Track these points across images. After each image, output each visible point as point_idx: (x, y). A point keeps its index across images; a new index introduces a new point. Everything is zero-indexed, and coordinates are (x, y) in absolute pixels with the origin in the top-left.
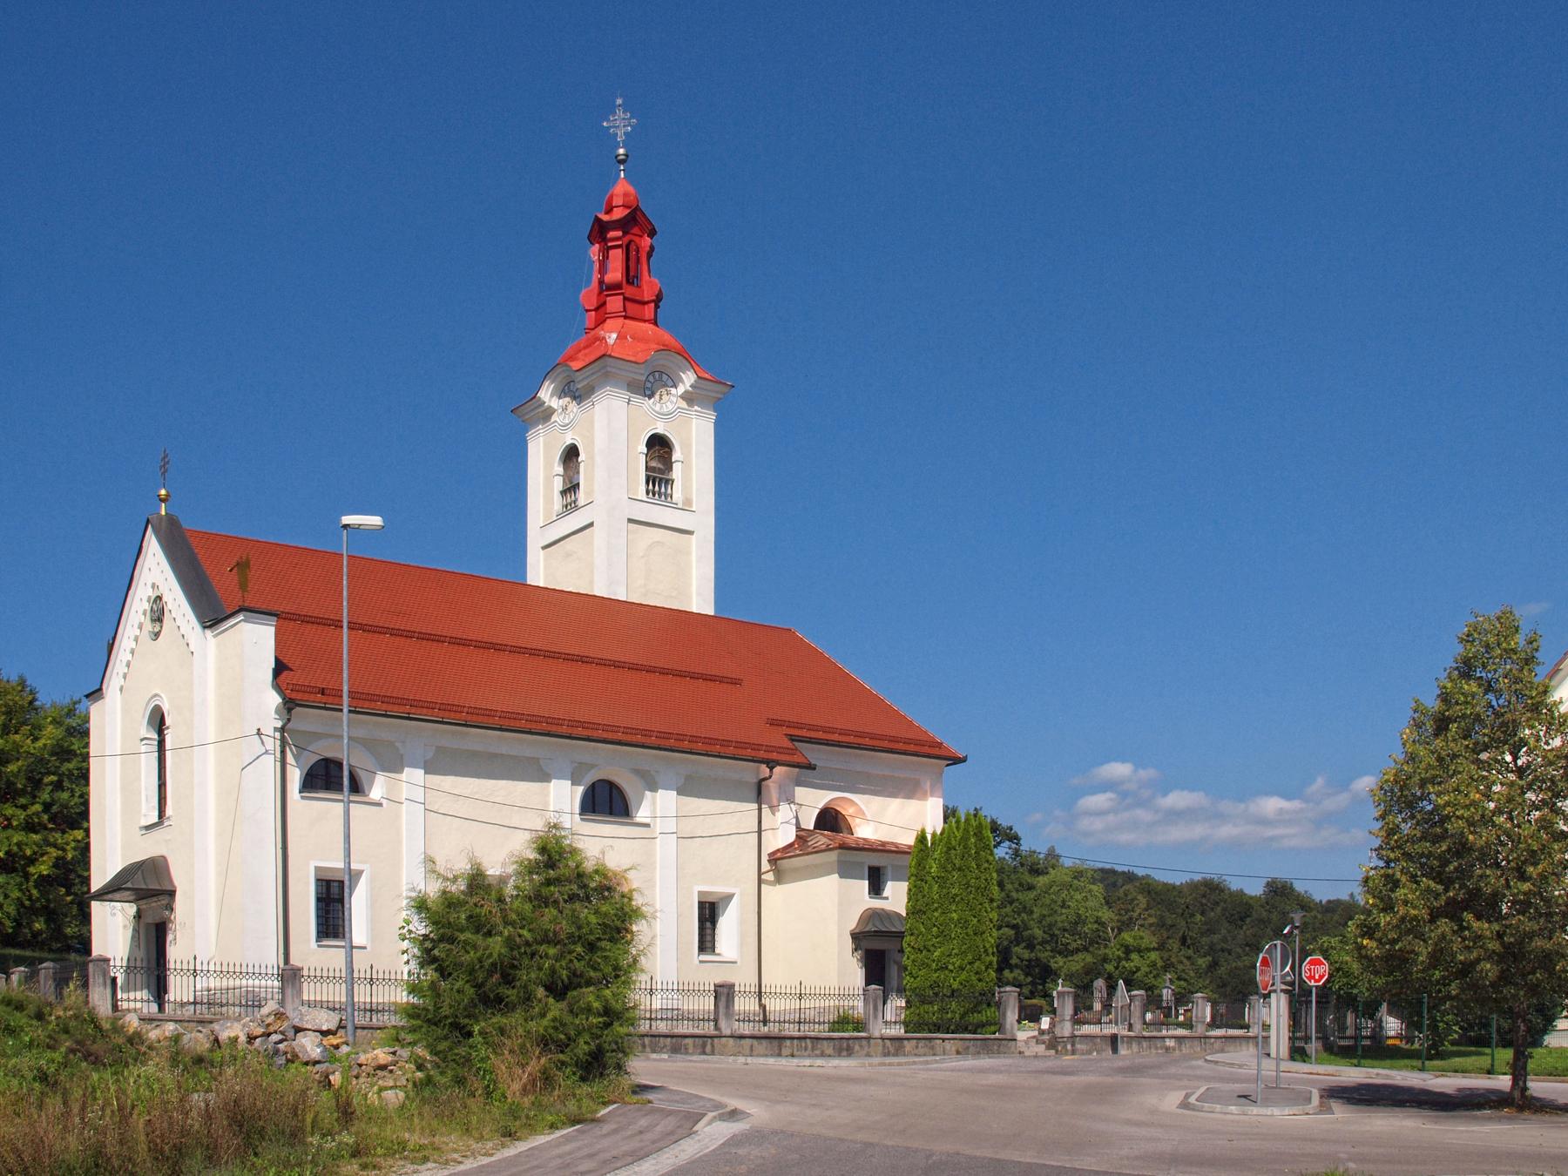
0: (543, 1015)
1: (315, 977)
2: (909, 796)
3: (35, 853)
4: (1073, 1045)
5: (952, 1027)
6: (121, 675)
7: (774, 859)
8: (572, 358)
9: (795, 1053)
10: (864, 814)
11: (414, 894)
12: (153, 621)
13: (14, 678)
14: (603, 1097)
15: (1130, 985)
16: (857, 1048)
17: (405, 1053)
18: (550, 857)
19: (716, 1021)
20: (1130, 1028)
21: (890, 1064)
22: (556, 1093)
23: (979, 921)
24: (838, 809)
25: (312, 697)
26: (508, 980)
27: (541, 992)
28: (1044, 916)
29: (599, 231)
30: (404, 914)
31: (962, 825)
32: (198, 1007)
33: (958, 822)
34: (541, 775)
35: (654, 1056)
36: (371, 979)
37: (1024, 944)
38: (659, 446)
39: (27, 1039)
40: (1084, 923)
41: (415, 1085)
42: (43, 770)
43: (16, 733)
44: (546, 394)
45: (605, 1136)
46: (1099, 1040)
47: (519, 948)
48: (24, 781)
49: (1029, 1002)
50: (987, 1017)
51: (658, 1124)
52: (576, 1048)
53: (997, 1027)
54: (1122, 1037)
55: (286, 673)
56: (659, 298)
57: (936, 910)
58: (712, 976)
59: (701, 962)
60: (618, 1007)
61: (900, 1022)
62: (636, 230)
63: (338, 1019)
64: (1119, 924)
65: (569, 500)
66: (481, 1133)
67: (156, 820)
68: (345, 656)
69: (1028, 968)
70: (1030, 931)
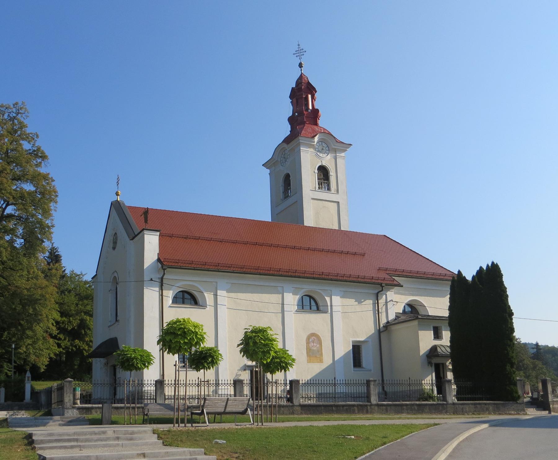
1: (228, 384)
19: (156, 399)
30: (93, 345)
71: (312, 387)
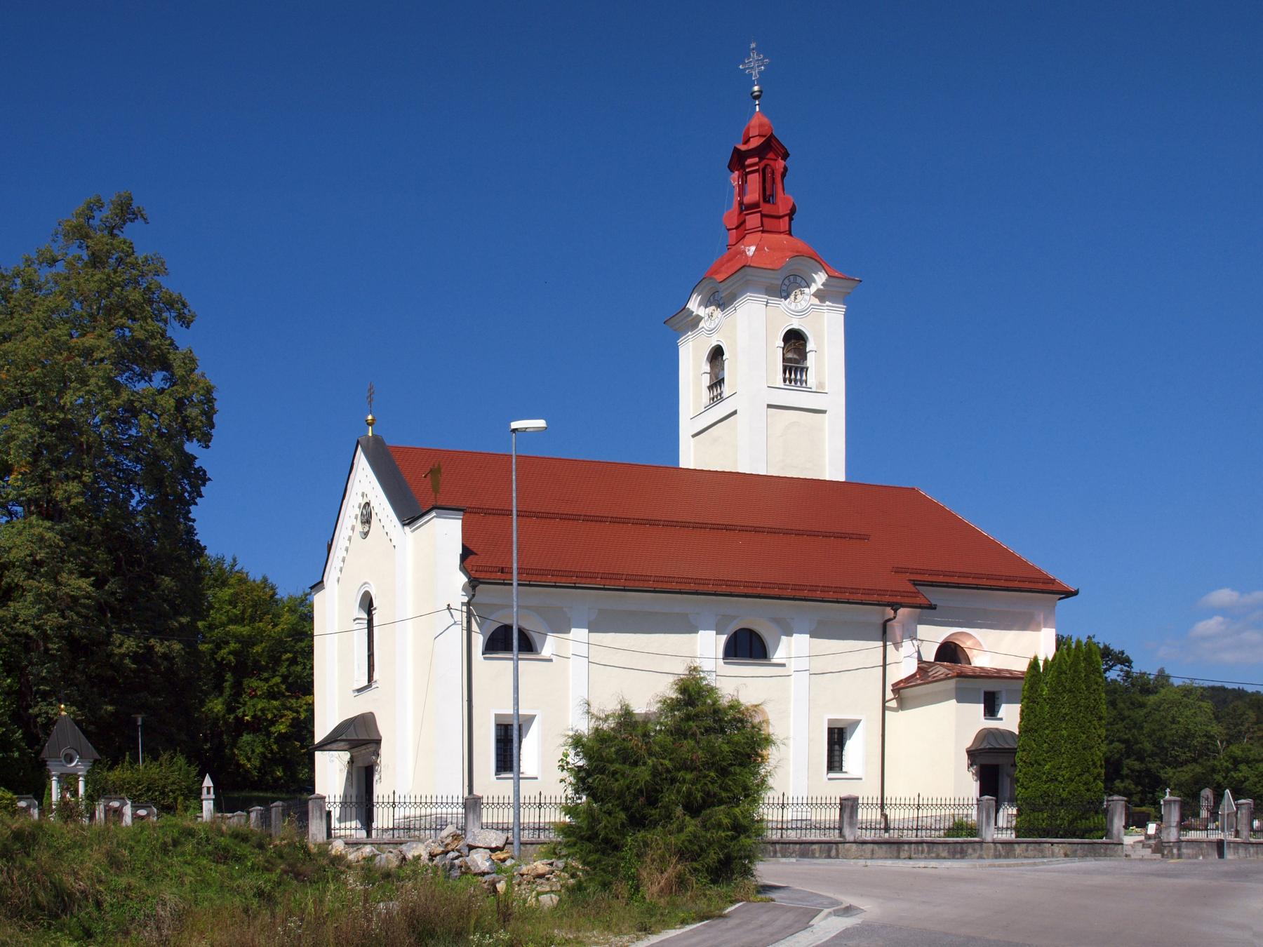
0: (680, 830)
2: (1024, 627)
3: (275, 716)
4: (1179, 849)
5: (1061, 832)
6: (338, 569)
7: (897, 688)
8: (716, 272)
9: (913, 856)
10: (981, 645)
11: (571, 733)
12: (363, 523)
13: (259, 579)
14: (730, 896)
15: (1237, 794)
16: (970, 851)
17: (561, 864)
18: (690, 696)
19: (841, 829)
20: (1237, 834)
21: (999, 866)
22: (689, 893)
23: (1087, 737)
24: (957, 642)
25: (493, 575)
26: (652, 802)
27: (679, 811)
28: (1154, 730)
29: (738, 160)
30: (563, 749)
31: (1073, 653)
32: (396, 832)
33: (1069, 648)
34: (688, 626)
35: (784, 860)
36: (540, 804)
37: (1134, 757)
38: (795, 340)
39: (249, 864)
40: (1193, 736)
41: (568, 889)
42: (281, 650)
43: (260, 621)
44: (694, 305)
45: (732, 928)
46: (1205, 845)
47: (661, 774)
48: (266, 659)
49: (1138, 809)
50: (1094, 823)
51: (777, 920)
52: (707, 858)
53: (1104, 832)
54: (1229, 843)
55: (471, 557)
56: (793, 210)
57: (1047, 728)
58: (840, 789)
59: (829, 779)
60: (745, 822)
61: (1011, 828)
62: (771, 155)
63: (505, 838)
64: (1228, 737)
65: (715, 393)
66: (620, 929)
67: (366, 683)
68: (515, 539)
69: (1138, 777)
70: (1140, 745)
71: (823, 809)
